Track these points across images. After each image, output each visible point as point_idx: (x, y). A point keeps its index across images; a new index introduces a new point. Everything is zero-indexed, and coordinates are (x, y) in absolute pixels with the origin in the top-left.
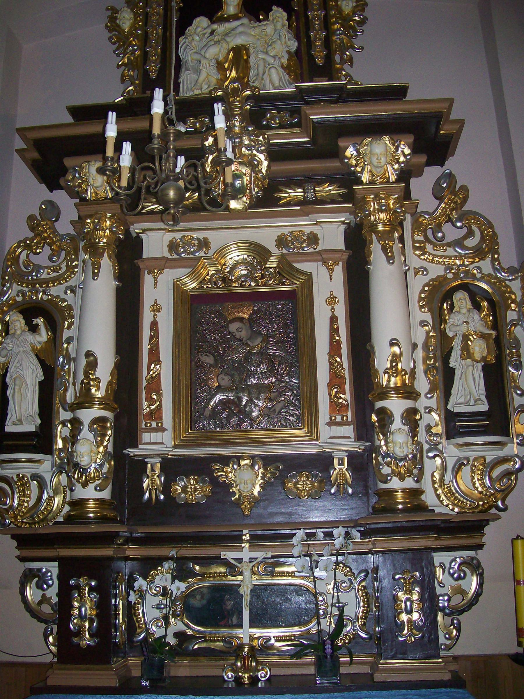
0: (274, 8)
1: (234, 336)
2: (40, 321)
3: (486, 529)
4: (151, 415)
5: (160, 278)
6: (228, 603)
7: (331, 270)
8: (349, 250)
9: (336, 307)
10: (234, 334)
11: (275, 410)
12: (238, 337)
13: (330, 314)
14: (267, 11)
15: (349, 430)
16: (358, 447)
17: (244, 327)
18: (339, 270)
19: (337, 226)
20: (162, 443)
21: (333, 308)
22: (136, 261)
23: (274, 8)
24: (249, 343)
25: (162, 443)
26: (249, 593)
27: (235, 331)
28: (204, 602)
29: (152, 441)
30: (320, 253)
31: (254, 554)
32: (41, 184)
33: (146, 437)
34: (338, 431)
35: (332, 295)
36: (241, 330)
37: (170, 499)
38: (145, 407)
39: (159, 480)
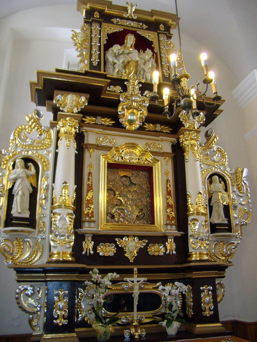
0: (148, 49)
1: (123, 183)
2: (30, 164)
3: (226, 270)
6: (122, 301)
11: (140, 217)
12: (124, 184)
13: (166, 179)
14: (144, 51)
15: (174, 227)
16: (179, 234)
17: (127, 180)
23: (148, 49)
26: (138, 297)
28: (112, 301)
30: (163, 153)
31: (139, 279)
32: (32, 100)
33: (86, 224)
36: (126, 181)
37: (96, 253)
39: (91, 245)
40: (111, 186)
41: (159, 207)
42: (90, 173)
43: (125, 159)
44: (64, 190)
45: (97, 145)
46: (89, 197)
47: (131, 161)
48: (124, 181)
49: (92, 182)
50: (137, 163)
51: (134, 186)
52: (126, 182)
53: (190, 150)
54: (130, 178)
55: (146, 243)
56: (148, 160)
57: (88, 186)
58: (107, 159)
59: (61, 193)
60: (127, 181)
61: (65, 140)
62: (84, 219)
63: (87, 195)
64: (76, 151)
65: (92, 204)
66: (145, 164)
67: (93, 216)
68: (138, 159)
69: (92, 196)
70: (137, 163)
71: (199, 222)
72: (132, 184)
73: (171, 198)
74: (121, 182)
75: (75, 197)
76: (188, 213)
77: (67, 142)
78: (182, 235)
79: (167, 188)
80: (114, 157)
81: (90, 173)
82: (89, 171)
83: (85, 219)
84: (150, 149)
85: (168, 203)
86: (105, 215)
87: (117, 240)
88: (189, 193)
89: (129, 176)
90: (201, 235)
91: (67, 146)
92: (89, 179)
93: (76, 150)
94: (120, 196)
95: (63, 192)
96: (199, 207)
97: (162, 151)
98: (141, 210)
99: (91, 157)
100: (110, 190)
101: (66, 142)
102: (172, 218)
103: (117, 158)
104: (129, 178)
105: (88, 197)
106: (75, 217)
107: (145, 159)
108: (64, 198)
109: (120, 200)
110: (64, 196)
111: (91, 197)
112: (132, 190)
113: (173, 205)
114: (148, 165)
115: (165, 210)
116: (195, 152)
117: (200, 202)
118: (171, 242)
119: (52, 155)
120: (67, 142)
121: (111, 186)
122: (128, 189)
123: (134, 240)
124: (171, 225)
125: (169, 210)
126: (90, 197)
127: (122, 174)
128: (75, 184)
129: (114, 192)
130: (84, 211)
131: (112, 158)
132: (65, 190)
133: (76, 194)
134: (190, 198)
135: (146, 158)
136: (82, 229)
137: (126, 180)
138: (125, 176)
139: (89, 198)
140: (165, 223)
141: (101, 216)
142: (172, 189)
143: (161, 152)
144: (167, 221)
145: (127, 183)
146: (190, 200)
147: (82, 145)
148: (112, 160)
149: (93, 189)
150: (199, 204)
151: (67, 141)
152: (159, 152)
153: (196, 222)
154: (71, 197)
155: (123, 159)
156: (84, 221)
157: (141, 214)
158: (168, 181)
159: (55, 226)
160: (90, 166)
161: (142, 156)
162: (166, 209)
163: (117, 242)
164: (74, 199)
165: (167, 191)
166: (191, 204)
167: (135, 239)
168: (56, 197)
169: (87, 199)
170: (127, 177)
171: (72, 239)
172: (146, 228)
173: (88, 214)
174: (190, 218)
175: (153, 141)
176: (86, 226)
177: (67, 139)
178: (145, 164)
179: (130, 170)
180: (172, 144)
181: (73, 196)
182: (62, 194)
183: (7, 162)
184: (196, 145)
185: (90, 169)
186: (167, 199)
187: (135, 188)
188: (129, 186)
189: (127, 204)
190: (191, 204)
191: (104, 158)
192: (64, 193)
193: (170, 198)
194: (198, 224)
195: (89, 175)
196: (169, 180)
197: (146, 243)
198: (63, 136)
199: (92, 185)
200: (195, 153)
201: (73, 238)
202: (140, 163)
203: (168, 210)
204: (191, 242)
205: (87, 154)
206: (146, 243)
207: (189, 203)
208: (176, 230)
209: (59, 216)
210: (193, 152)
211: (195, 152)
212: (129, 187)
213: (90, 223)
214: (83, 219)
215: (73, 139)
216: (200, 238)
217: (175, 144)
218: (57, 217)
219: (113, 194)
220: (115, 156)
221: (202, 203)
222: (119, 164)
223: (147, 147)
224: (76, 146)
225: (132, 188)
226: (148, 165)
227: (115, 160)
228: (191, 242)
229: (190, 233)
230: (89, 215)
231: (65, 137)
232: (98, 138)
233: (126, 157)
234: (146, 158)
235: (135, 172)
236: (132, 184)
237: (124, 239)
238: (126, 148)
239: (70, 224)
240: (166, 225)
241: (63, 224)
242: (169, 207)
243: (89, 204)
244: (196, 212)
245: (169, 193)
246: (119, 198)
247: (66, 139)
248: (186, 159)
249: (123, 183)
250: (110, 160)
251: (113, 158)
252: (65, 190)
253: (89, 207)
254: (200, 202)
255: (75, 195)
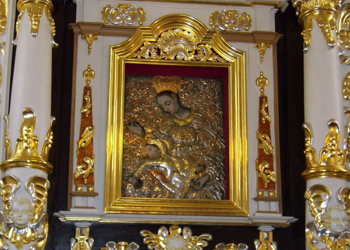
1: (162, 109)
4: (83, 179)
5: (94, 44)
7: (263, 52)
8: (279, 33)
9: (265, 88)
10: (162, 107)
11: (199, 183)
13: (259, 94)
15: (275, 206)
18: (270, 53)
19: (269, 9)
20: (93, 208)
21: (262, 88)
22: (70, 24)
24: (176, 115)
25: (93, 208)
27: (163, 104)
29: (89, 205)
30: (253, 34)
33: (77, 201)
34: (263, 206)
35: (262, 75)
36: (168, 103)
38: (78, 170)
40: (136, 116)
41: (240, 160)
42: (87, 90)
43: (165, 53)
44: (25, 128)
45: (103, 26)
46: (85, 142)
47: (178, 57)
48: (165, 103)
49: (91, 109)
50: (192, 62)
51: (187, 114)
52: (169, 105)
53: (314, 22)
54: (177, 96)
55: (208, 242)
56: (217, 54)
57: (82, 118)
58: (125, 56)
59: (20, 135)
60: (170, 102)
61: (29, 17)
62: (74, 190)
63: (81, 138)
64: (54, 42)
65: (91, 157)
66: (170, 61)
67: (92, 183)
68: (194, 53)
69: (92, 139)
70: (192, 62)
71: (329, 194)
72: (182, 108)
73: (268, 138)
74: (158, 107)
75: (50, 141)
76: (304, 173)
77: (33, 23)
78: (292, 224)
79: (261, 115)
80: (139, 49)
81: (87, 90)
82: (85, 85)
83: (76, 189)
84: (223, 26)
85: (261, 151)
86: (120, 180)
87: (145, 235)
88: (309, 125)
89: (176, 92)
90: (334, 224)
91: (33, 31)
92: (85, 103)
93: (55, 39)
94: (156, 138)
95: (25, 132)
96: (332, 159)
97: (251, 31)
98: (201, 168)
99: (89, 52)
100: (135, 125)
101: (31, 21)
102: (268, 184)
103: (147, 53)
104: (175, 96)
105: (82, 140)
106: (49, 186)
107: (211, 52)
108: (25, 145)
109: (155, 145)
110: (26, 141)
111: (88, 140)
112: (182, 124)
113: (274, 154)
114: (218, 63)
115: (254, 166)
116: (328, 28)
117: (334, 145)
118: (267, 239)
119: (5, 53)
120: (33, 23)
121: (136, 116)
122: (174, 122)
123: (181, 234)
124: (268, 199)
125: (263, 168)
126: (87, 140)
127: (160, 87)
128: (53, 114)
129: (142, 128)
130: (74, 173)
131: (136, 52)
132: (29, 127)
133: (53, 135)
134: (309, 139)
135: (212, 49)
136: (69, 210)
137: (170, 102)
138: (168, 93)
139: (84, 144)
140: (255, 195)
141: (110, 180)
142: (272, 117)
143: (248, 32)
144: (258, 192)
145: (171, 107)
146: (309, 143)
147: (71, 26)
148: (136, 57)
149: (94, 125)
150: (332, 150)
151: (33, 19)
152: (244, 31)
153: (322, 194)
154: (41, 143)
155: (161, 53)
156: (73, 195)
157: (202, 176)
158: (263, 99)
159: (6, 206)
160: (89, 73)
161: (205, 44)
162: (258, 164)
163: (145, 240)
164: (50, 146)
165: (260, 122)
166: (311, 151)
167: (184, 232)
168: (11, 144)
169: (80, 147)
170: (172, 94)
171: (43, 233)
172: (208, 208)
173: (81, 179)
174: (311, 183)
175: (232, 8)
176: (77, 205)
177: (32, 15)
178: (170, 61)
179: (178, 78)
180: (275, 11)
181: (48, 140)
182: (22, 137)
183: (261, 74)
184: (332, 10)
185: (88, 80)
186: (260, 142)
187: (188, 118)
188: (176, 115)
189: (171, 156)
190: (311, 151)
191: (117, 53)
192: (26, 135)
193: (265, 139)
194: (327, 197)
195: (85, 94)
196: (266, 98)
197: (208, 242)
198: (24, 9)
199: (91, 114)
200: (327, 31)
201: (46, 231)
202: (198, 60)
203: (260, 166)
204: (309, 240)
205: (81, 45)
206: (209, 242)
207: (308, 150)
208: (280, 213)
209: (15, 185)
210: (321, 27)
211: (328, 28)
212: (175, 117)
213: (85, 198)
214: (72, 189)
215: (47, 13)
216: (331, 230)
217: (283, 10)
218: (11, 187)
219: (140, 133)
220: (142, 49)
221: (338, 150)
222: (182, 66)
223: (217, 24)
224: (55, 29)
225: (183, 118)
226: (218, 63)
227: (142, 58)
228: (309, 240)
229: (309, 218)
230: (84, 182)
231: (29, 11)
232: (105, 8)
233: (166, 50)
234: (212, 49)
235: (190, 82)
236: (182, 108)
237: (160, 231)
238: (166, 29)
239: (39, 202)
240: (257, 199)
241: (21, 201)
242: (264, 160)
243: (84, 157)
244: (324, 171)
245: (264, 128)
246: (152, 142)
247: (29, 15)
248: (306, 46)
249: (162, 109)
250: (133, 58)
251: (139, 52)
252: (29, 127)
253: (84, 163)
254: (334, 145)
255: (51, 137)
